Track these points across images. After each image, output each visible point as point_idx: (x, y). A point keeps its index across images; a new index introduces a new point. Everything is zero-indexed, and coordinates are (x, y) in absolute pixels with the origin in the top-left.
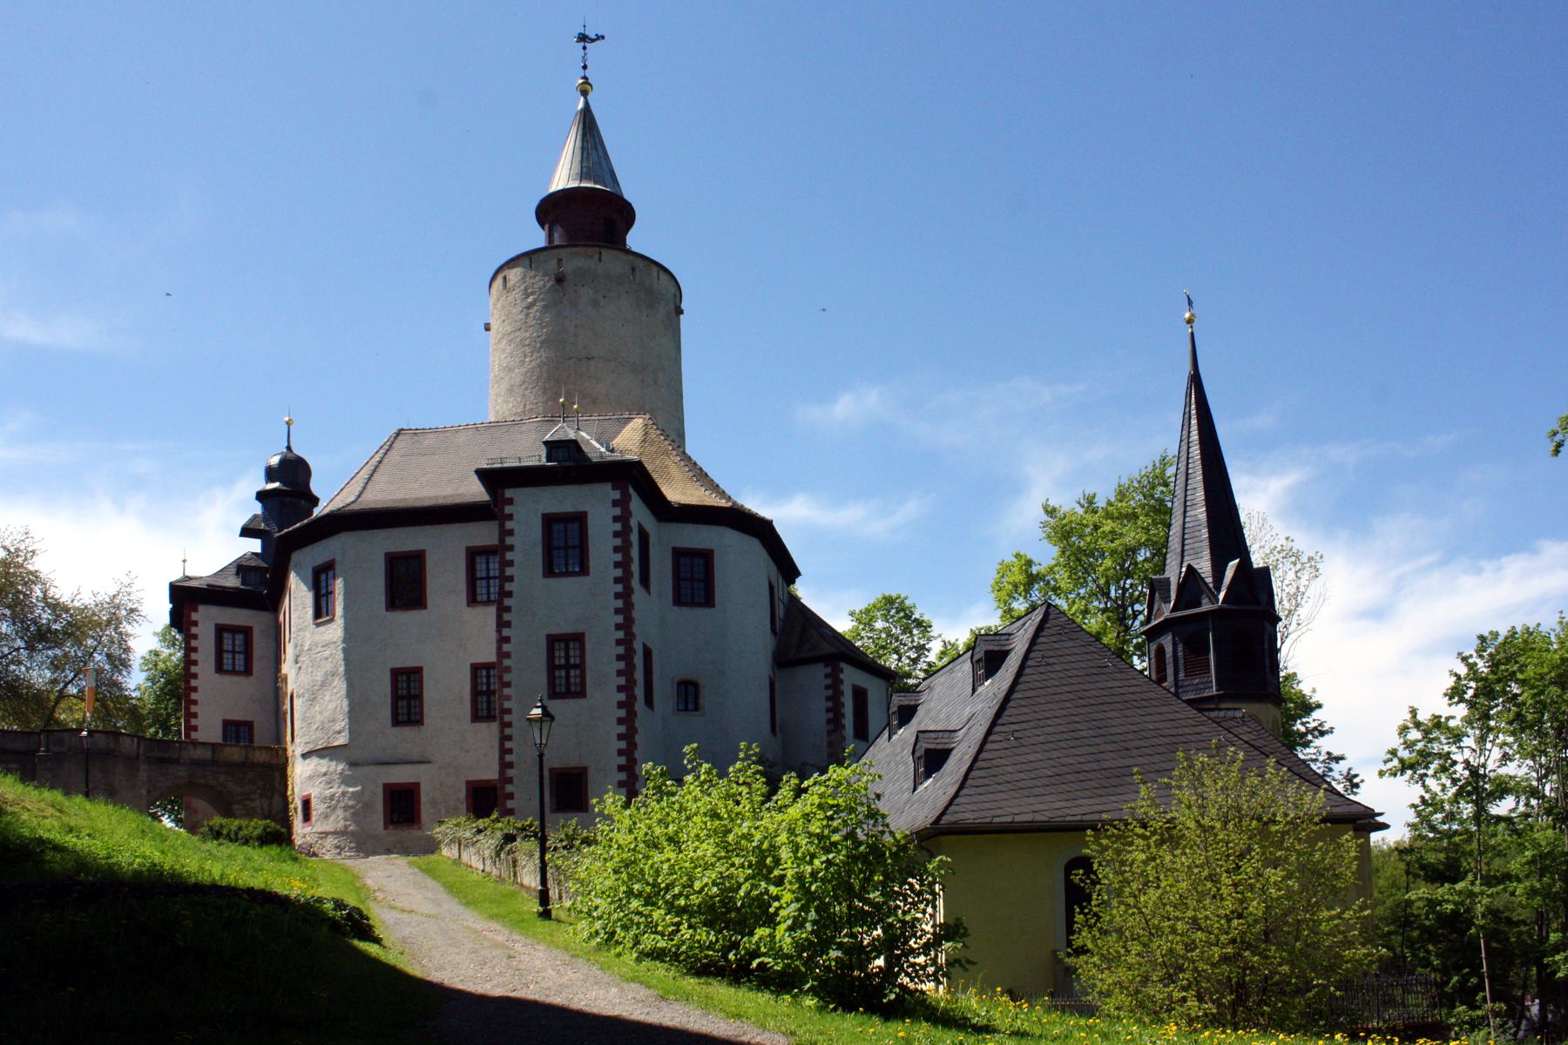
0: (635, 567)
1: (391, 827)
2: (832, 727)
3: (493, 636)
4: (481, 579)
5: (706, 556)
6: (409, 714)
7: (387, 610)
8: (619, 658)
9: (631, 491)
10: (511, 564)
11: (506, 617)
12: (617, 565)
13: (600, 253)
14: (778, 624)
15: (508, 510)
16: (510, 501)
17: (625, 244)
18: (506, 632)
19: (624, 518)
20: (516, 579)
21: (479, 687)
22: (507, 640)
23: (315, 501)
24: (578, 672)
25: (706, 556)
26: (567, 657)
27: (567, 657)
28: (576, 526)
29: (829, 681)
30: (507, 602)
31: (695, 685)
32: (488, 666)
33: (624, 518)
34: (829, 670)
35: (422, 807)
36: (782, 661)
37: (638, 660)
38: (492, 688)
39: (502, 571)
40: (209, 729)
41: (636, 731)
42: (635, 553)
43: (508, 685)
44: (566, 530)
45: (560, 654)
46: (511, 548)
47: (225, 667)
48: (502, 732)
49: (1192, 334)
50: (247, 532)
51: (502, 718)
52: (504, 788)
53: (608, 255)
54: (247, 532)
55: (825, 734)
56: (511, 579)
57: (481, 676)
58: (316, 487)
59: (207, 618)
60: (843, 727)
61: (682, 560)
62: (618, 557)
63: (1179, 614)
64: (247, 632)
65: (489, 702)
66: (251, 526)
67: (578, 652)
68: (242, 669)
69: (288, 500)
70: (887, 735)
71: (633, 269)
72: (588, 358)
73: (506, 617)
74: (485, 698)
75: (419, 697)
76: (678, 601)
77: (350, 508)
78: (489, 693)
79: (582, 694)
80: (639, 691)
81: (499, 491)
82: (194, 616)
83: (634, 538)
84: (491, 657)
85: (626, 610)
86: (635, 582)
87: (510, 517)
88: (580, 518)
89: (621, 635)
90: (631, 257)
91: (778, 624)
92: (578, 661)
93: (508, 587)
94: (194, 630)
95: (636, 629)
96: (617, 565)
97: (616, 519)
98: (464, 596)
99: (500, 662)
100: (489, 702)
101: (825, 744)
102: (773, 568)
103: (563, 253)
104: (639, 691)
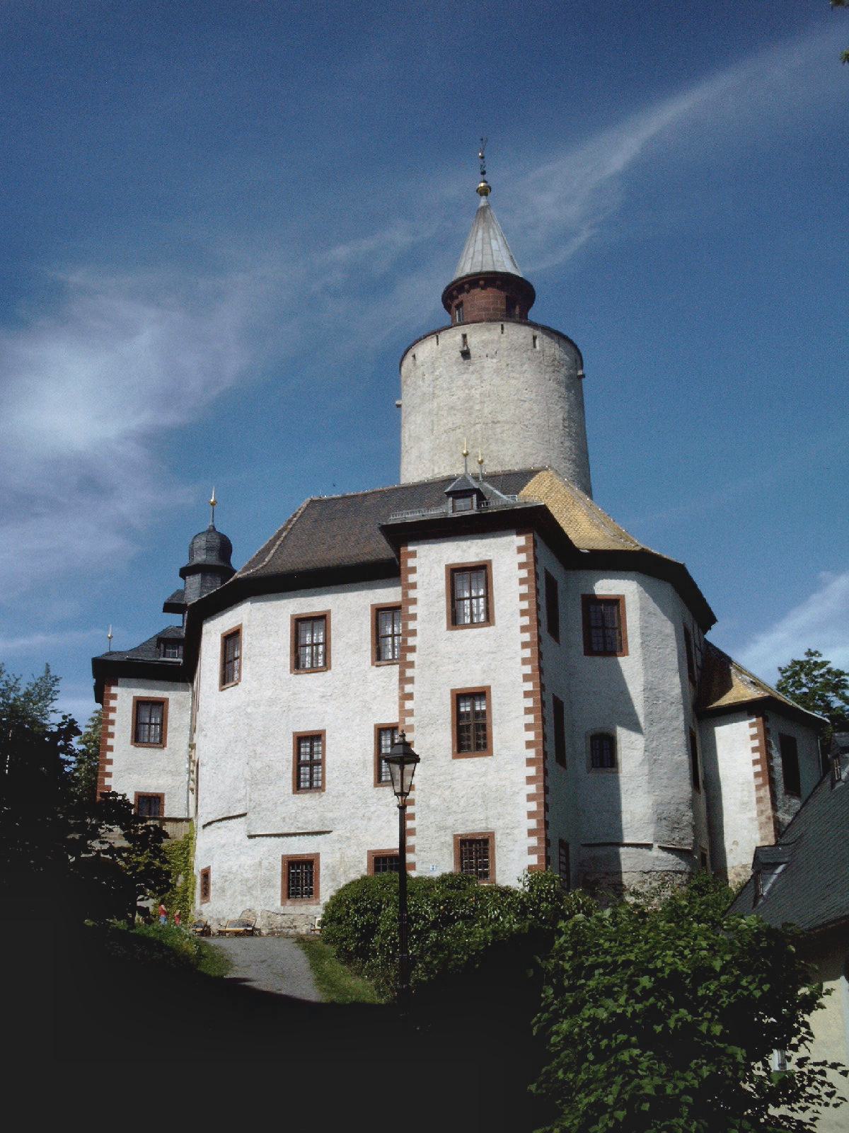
1: (289, 902)
11: (409, 673)
13: (502, 325)
16: (413, 554)
20: (418, 632)
22: (409, 696)
23: (233, 572)
32: (392, 729)
50: (169, 607)
54: (169, 607)
66: (172, 602)
70: (829, 783)
72: (493, 422)
73: (409, 673)
75: (320, 763)
94: (112, 703)
98: (369, 654)
99: (403, 721)
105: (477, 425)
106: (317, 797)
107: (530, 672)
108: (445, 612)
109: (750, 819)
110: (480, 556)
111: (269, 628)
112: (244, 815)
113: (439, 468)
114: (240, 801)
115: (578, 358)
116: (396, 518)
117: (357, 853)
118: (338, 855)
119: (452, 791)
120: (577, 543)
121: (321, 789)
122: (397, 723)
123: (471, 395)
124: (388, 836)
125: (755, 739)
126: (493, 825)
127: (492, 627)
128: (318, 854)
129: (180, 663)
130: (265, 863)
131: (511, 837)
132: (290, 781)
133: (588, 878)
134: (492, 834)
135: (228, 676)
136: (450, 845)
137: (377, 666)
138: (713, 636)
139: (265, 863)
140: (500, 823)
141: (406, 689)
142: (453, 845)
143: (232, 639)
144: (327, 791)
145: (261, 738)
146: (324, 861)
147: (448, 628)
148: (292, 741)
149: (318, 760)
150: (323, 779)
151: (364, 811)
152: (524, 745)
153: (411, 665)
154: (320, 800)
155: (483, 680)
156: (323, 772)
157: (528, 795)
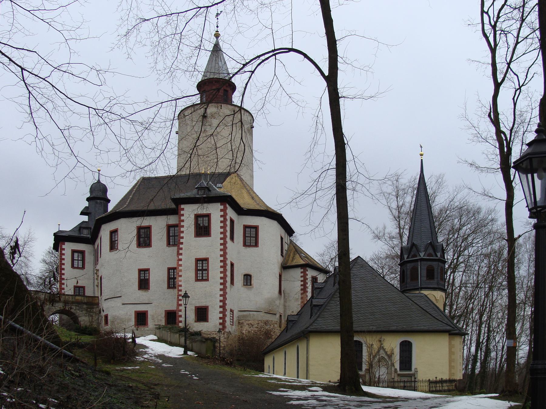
2: (302, 292)
5: (256, 228)
9: (227, 205)
11: (181, 252)
16: (183, 209)
18: (180, 257)
21: (170, 276)
22: (181, 260)
24: (206, 272)
25: (256, 228)
26: (202, 266)
27: (202, 266)
28: (207, 219)
29: (302, 274)
31: (250, 276)
32: (174, 269)
33: (224, 216)
34: (302, 270)
35: (149, 319)
36: (285, 267)
37: (228, 267)
38: (175, 276)
40: (69, 290)
41: (226, 293)
42: (228, 228)
43: (181, 276)
45: (200, 265)
47: (75, 266)
49: (422, 160)
50: (82, 213)
51: (178, 288)
54: (82, 213)
59: (68, 247)
60: (307, 292)
61: (247, 229)
63: (402, 262)
64: (82, 253)
65: (174, 282)
66: (84, 211)
67: (206, 265)
68: (81, 267)
69: (99, 201)
74: (172, 281)
76: (245, 245)
78: (174, 278)
81: (179, 206)
82: (64, 247)
83: (228, 223)
84: (175, 266)
85: (224, 250)
88: (208, 216)
90: (233, 107)
91: (284, 252)
92: (206, 268)
95: (227, 256)
98: (165, 242)
100: (174, 282)
107: (223, 254)
108: (194, 231)
116: (177, 196)
120: (242, 206)
126: (207, 304)
130: (129, 313)
135: (113, 246)
139: (129, 313)
140: (210, 303)
143: (114, 233)
146: (150, 314)
147: (195, 237)
148: (138, 271)
157: (220, 295)
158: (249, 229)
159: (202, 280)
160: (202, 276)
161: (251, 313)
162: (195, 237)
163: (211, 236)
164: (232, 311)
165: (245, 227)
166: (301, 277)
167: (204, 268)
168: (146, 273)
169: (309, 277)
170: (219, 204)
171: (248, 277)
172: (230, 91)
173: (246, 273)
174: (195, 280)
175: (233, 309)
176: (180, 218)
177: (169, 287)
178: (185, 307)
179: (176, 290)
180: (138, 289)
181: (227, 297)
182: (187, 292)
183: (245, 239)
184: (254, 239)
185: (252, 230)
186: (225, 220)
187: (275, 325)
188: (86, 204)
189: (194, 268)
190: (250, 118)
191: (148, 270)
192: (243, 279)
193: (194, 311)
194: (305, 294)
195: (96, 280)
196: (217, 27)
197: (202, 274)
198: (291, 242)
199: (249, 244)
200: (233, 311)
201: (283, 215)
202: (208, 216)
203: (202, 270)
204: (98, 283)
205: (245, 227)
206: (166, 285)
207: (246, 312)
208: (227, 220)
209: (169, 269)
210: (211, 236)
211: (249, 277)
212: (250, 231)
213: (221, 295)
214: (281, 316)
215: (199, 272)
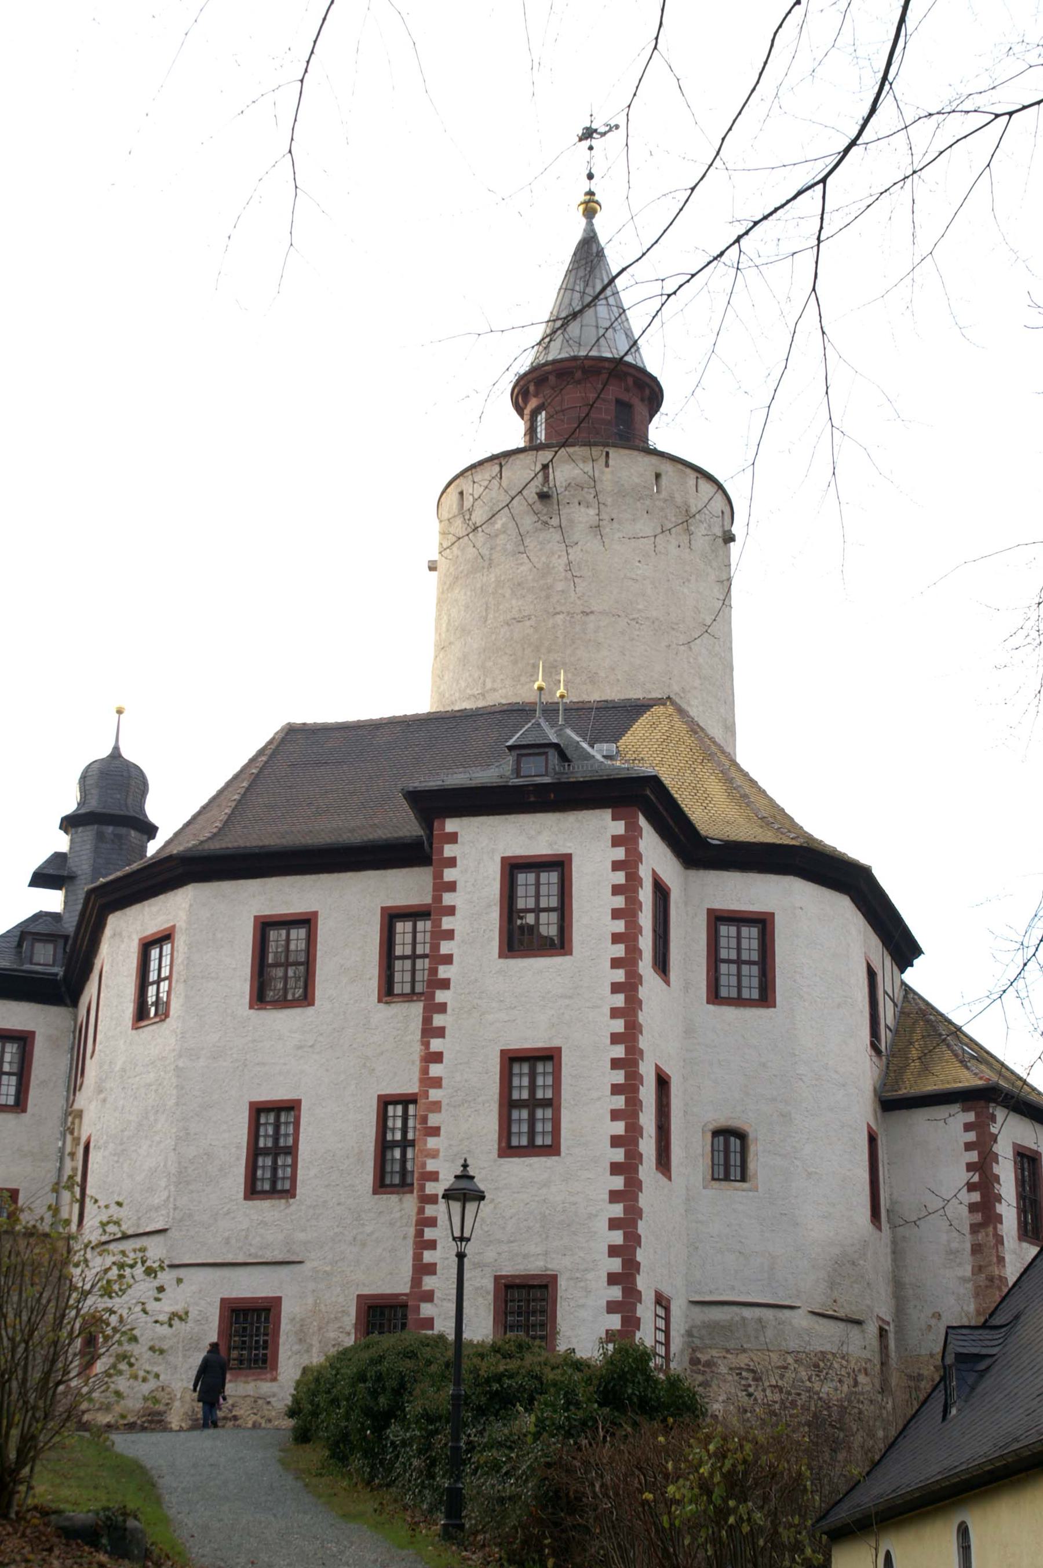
0: (646, 942)
2: (978, 1217)
3: (417, 1049)
4: (404, 957)
5: (763, 923)
6: (274, 1180)
7: (251, 1007)
8: (616, 1089)
9: (642, 821)
10: (450, 935)
11: (438, 1020)
12: (616, 938)
13: (607, 454)
14: (885, 1037)
15: (449, 851)
16: (453, 838)
17: (646, 439)
18: (436, 1045)
19: (629, 865)
20: (455, 959)
23: (151, 831)
24: (549, 1113)
25: (763, 923)
26: (533, 1087)
27: (533, 1087)
28: (554, 877)
30: (441, 996)
31: (741, 1136)
32: (406, 1101)
33: (629, 865)
34: (970, 1117)
35: (282, 1339)
37: (648, 1093)
39: (435, 947)
42: (646, 919)
43: (435, 1131)
44: (538, 884)
46: (451, 911)
48: (421, 1211)
50: (42, 879)
51: (422, 1188)
52: (418, 1309)
53: (620, 458)
54: (42, 879)
55: (966, 1230)
56: (448, 959)
57: (393, 1130)
58: (154, 810)
60: (999, 1218)
61: (723, 930)
62: (620, 926)
66: (45, 871)
67: (549, 1081)
71: (658, 476)
73: (438, 1020)
75: (292, 1151)
76: (715, 996)
77: (206, 846)
79: (553, 1149)
80: (648, 1146)
81: (436, 824)
83: (646, 895)
86: (646, 966)
87: (452, 862)
89: (617, 1210)
90: (654, 460)
91: (885, 1037)
92: (549, 1095)
93: (443, 972)
95: (643, 1043)
96: (616, 890)
97: (616, 866)
101: (968, 1246)
102: (875, 942)
103: (545, 456)
104: (648, 1146)
105: (558, 616)
106: (283, 1207)
109: (960, 1278)
110: (556, 847)
111: (219, 935)
112: (163, 1231)
113: (494, 681)
114: (157, 1209)
115: (727, 510)
117: (341, 1299)
118: (310, 1301)
119: (495, 1208)
121: (290, 1193)
122: (416, 1094)
123: (551, 565)
124: (391, 1274)
125: (973, 1150)
126: (554, 1265)
127: (567, 958)
128: (279, 1299)
129: (56, 975)
131: (582, 1284)
132: (241, 1180)
133: (699, 1356)
134: (554, 1278)
136: (488, 1293)
137: (386, 1003)
138: (915, 977)
141: (431, 1046)
142: (492, 1293)
144: (297, 1197)
145: (198, 1109)
146: (288, 1310)
147: (501, 956)
148: (246, 1114)
149: (544, 1099)
150: (293, 1178)
151: (355, 1232)
152: (608, 1142)
153: (442, 1008)
154: (287, 1211)
155: (550, 1039)
156: (294, 1166)
157: (611, 1220)
158: (733, 930)
159: (532, 1149)
160: (532, 1133)
161: (748, 1313)
162: (501, 956)
163: (570, 953)
164: (662, 1301)
165: (717, 919)
166: (969, 1147)
167: (540, 1095)
168: (283, 1119)
169: (1004, 1149)
170: (607, 814)
171: (732, 1139)
172: (640, 409)
173: (723, 1119)
174: (500, 1149)
175: (667, 1291)
176: (438, 875)
177: (381, 1185)
178: (461, 1256)
179: (410, 1202)
180: (242, 1195)
181: (640, 1231)
182: (471, 1171)
183: (717, 969)
184: (755, 970)
185: (745, 931)
186: (633, 881)
187: (862, 1378)
188: (62, 843)
189: (497, 1097)
190: (719, 503)
191: (292, 1107)
192: (709, 1148)
193: (491, 1297)
194: (991, 1229)
195: (67, 1159)
196: (590, 176)
197: (532, 1121)
198: (905, 997)
199: (734, 994)
200: (669, 1301)
201: (874, 871)
202: (560, 864)
203: (533, 1104)
204: (75, 1169)
205: (717, 919)
206: (367, 1177)
207: (726, 1308)
208: (640, 881)
209: (385, 1102)
210: (570, 953)
211: (735, 1143)
212: (739, 937)
213: (614, 1224)
214: (882, 1333)
215: (515, 1114)
